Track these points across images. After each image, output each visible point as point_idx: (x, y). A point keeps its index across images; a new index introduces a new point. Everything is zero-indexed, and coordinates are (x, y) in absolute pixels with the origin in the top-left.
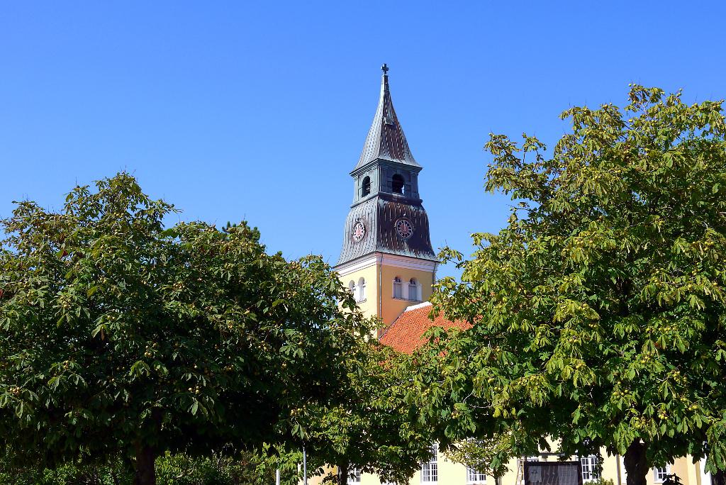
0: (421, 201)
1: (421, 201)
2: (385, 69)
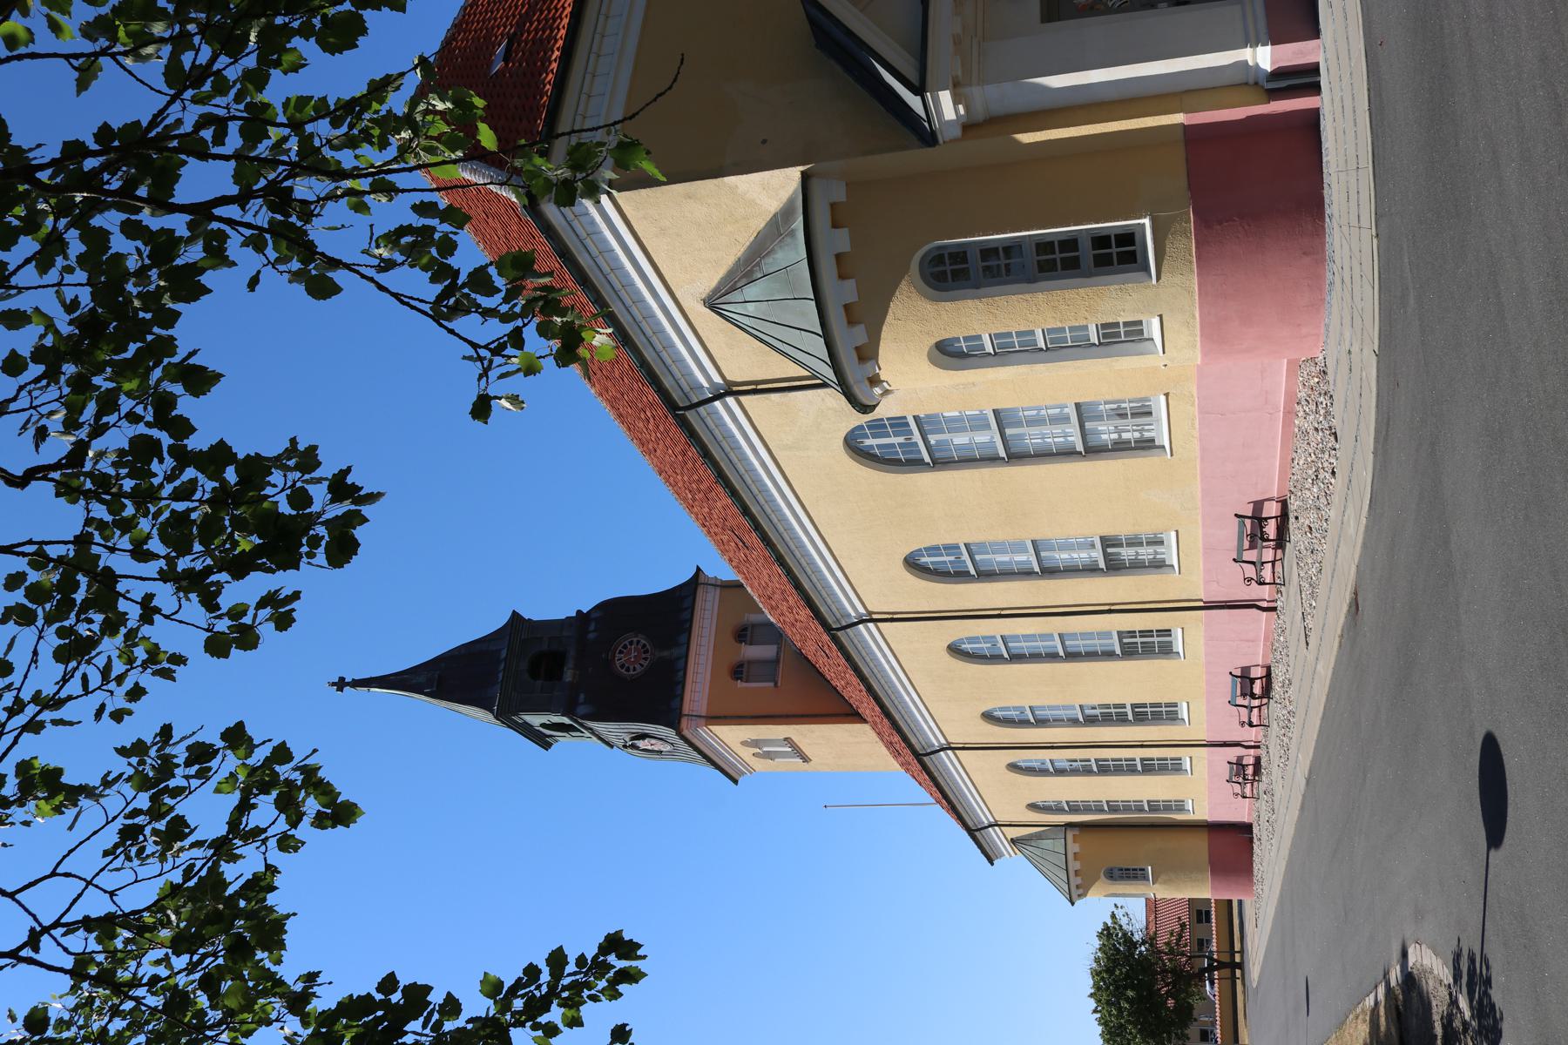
0: (579, 612)
1: (579, 612)
2: (341, 684)
